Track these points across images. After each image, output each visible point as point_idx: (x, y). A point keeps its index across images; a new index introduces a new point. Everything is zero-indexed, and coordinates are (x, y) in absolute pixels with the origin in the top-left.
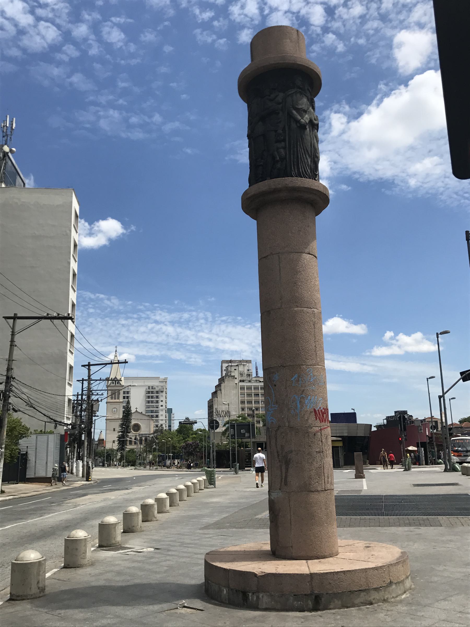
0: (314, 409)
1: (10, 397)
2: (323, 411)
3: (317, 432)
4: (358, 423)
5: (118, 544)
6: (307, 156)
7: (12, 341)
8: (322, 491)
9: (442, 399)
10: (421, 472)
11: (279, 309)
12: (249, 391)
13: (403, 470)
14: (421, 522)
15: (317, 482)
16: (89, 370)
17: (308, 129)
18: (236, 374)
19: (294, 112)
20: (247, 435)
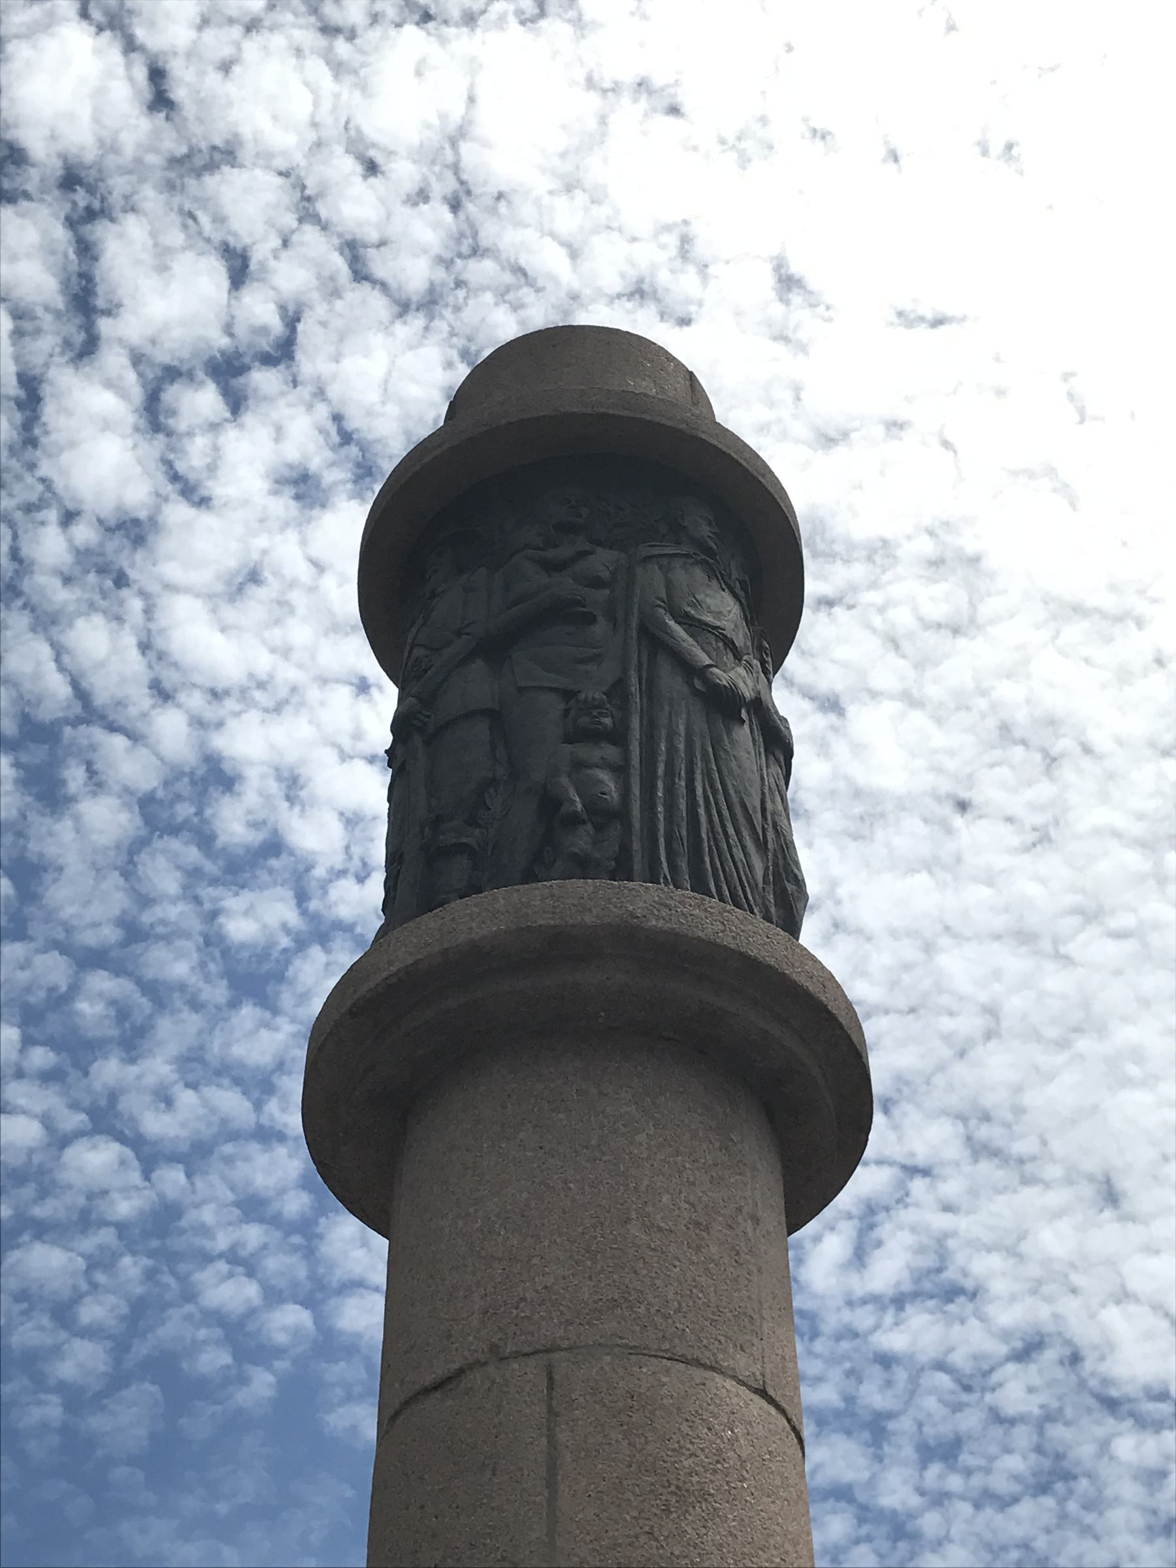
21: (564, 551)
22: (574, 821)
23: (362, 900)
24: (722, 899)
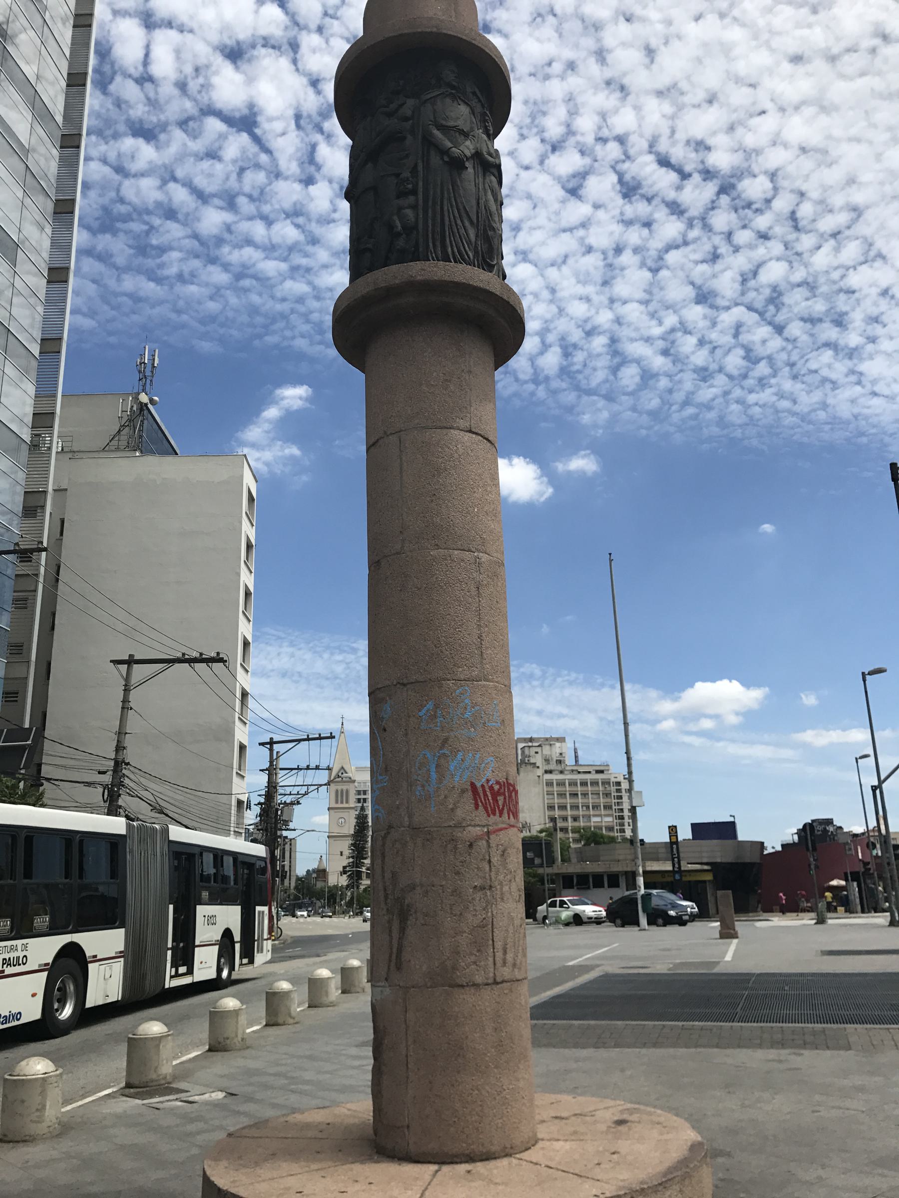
0: (472, 784)
1: (120, 795)
2: (496, 787)
3: (479, 838)
4: (741, 837)
5: (163, 1082)
6: (467, 224)
7: (125, 701)
8: (487, 984)
9: (878, 792)
10: (845, 925)
11: (398, 553)
12: (561, 789)
13: (814, 921)
14: (809, 1038)
15: (475, 963)
16: (271, 750)
17: (470, 170)
18: (538, 760)
19: (436, 132)
20: (537, 861)
21: (393, 106)
22: (399, 234)
23: (339, 279)
24: (456, 262)
